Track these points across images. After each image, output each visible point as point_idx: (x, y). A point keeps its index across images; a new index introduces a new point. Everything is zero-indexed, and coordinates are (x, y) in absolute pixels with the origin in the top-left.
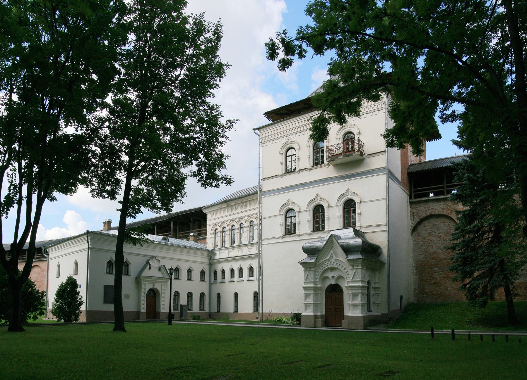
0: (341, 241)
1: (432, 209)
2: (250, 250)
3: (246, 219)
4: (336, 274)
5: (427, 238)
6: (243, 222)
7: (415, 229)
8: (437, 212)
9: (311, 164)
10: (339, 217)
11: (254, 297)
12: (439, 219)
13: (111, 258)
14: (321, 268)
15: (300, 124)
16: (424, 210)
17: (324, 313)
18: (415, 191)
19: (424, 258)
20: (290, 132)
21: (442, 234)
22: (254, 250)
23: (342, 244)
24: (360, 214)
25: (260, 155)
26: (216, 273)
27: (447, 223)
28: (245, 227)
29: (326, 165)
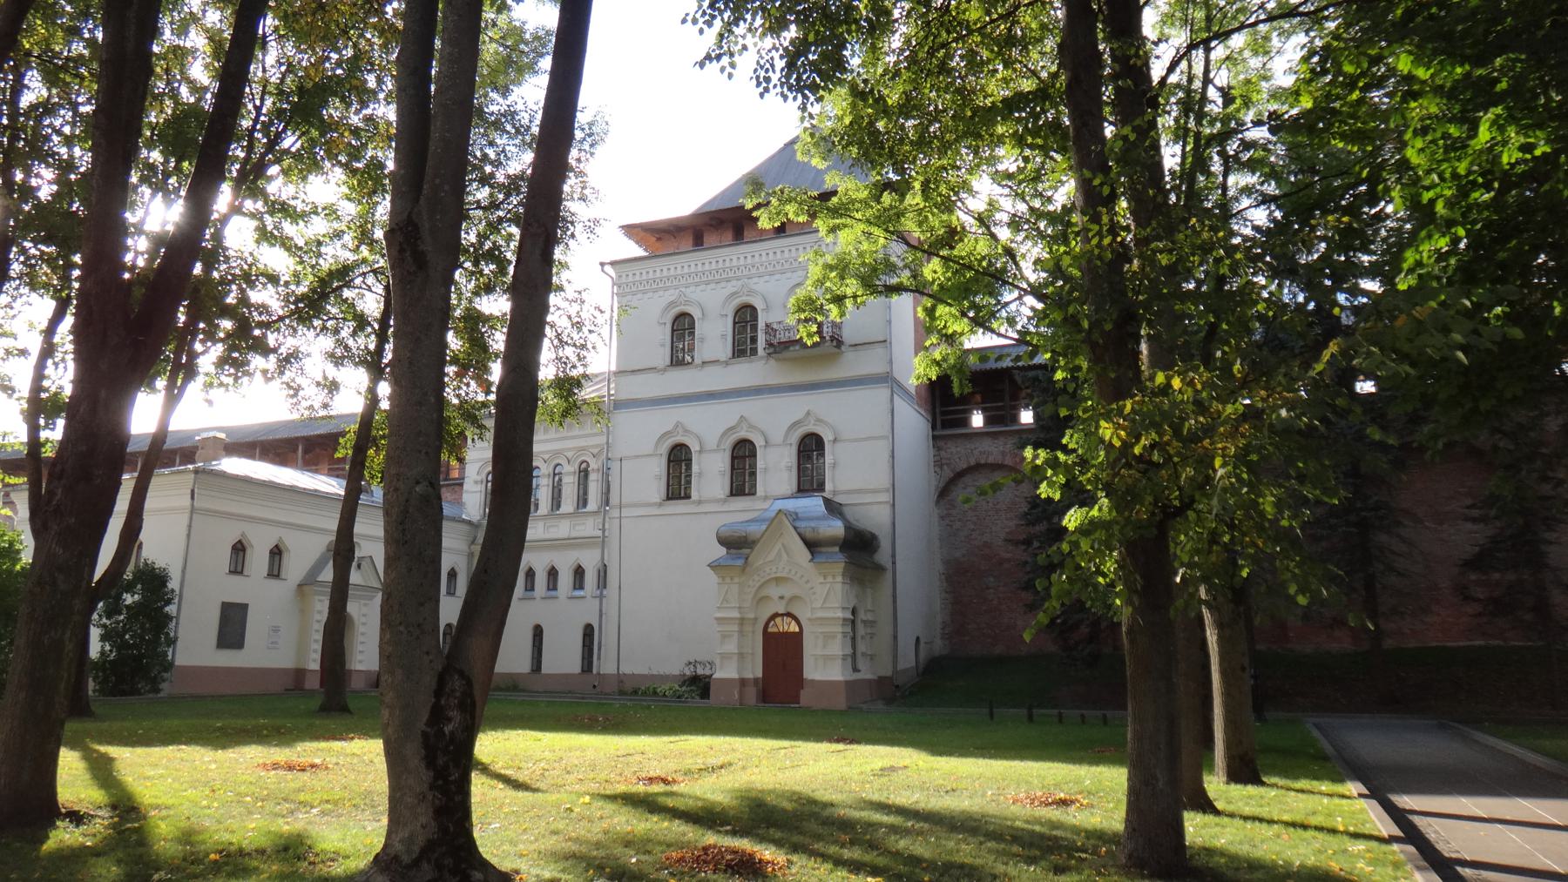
3: (570, 454)
4: (787, 591)
6: (563, 461)
7: (944, 493)
8: (991, 460)
9: (730, 354)
10: (789, 468)
11: (585, 635)
15: (707, 267)
17: (760, 675)
18: (943, 413)
22: (588, 528)
24: (834, 465)
28: (568, 474)
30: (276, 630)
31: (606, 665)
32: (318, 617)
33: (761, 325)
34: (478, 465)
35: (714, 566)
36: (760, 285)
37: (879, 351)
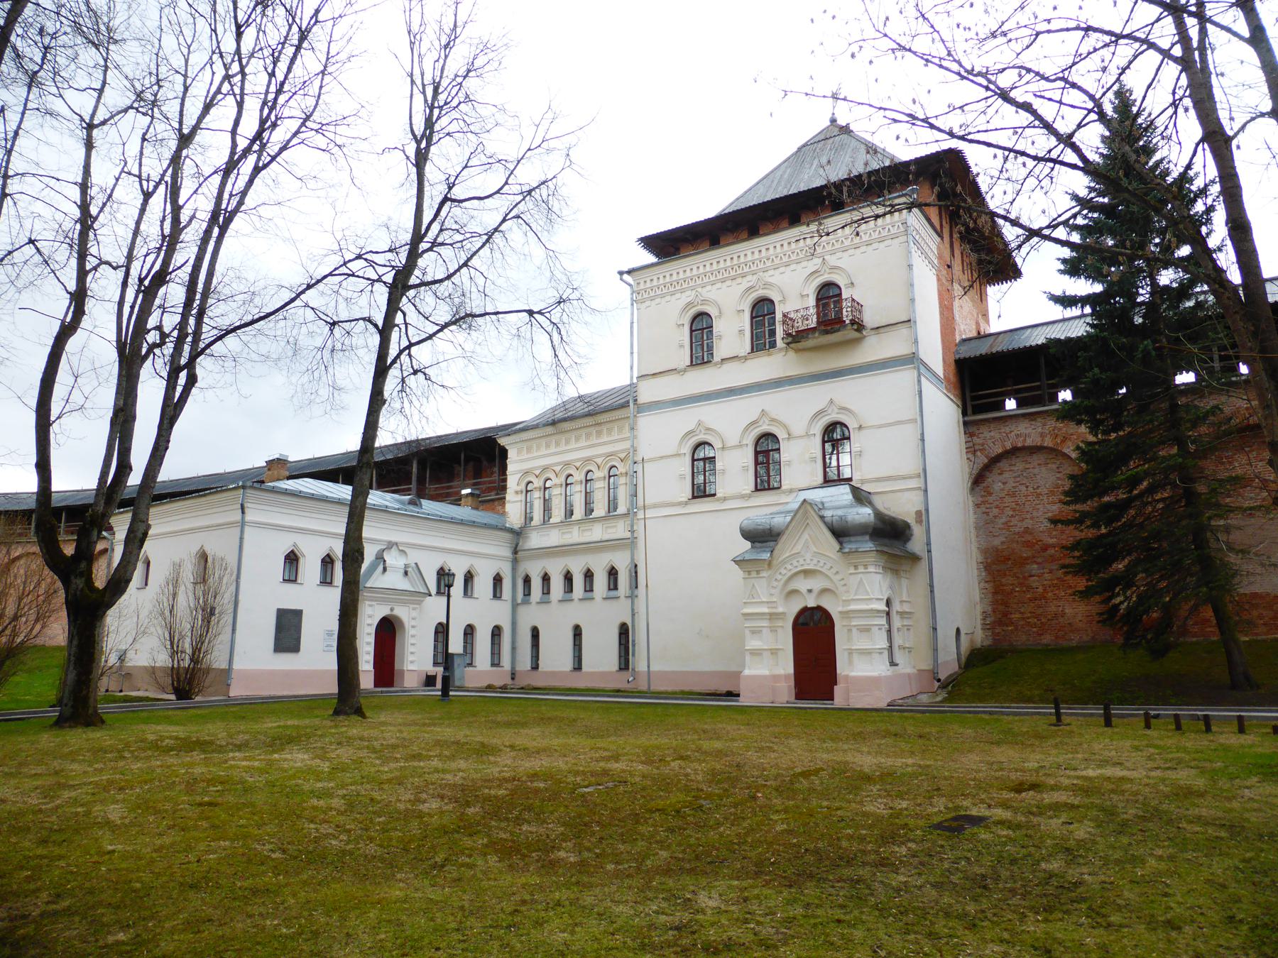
1: (1017, 436)
2: (610, 531)
4: (816, 584)
5: (1008, 499)
7: (978, 480)
8: (1029, 442)
9: (748, 349)
11: (620, 634)
12: (1035, 456)
13: (331, 549)
16: (995, 440)
18: (973, 399)
19: (1003, 543)
20: (699, 282)
21: (1041, 493)
22: (619, 530)
25: (632, 327)
26: (527, 580)
27: (1054, 466)
28: (599, 479)
29: (781, 349)
32: (369, 621)
33: (779, 316)
35: (739, 562)
36: (775, 277)
37: (904, 331)
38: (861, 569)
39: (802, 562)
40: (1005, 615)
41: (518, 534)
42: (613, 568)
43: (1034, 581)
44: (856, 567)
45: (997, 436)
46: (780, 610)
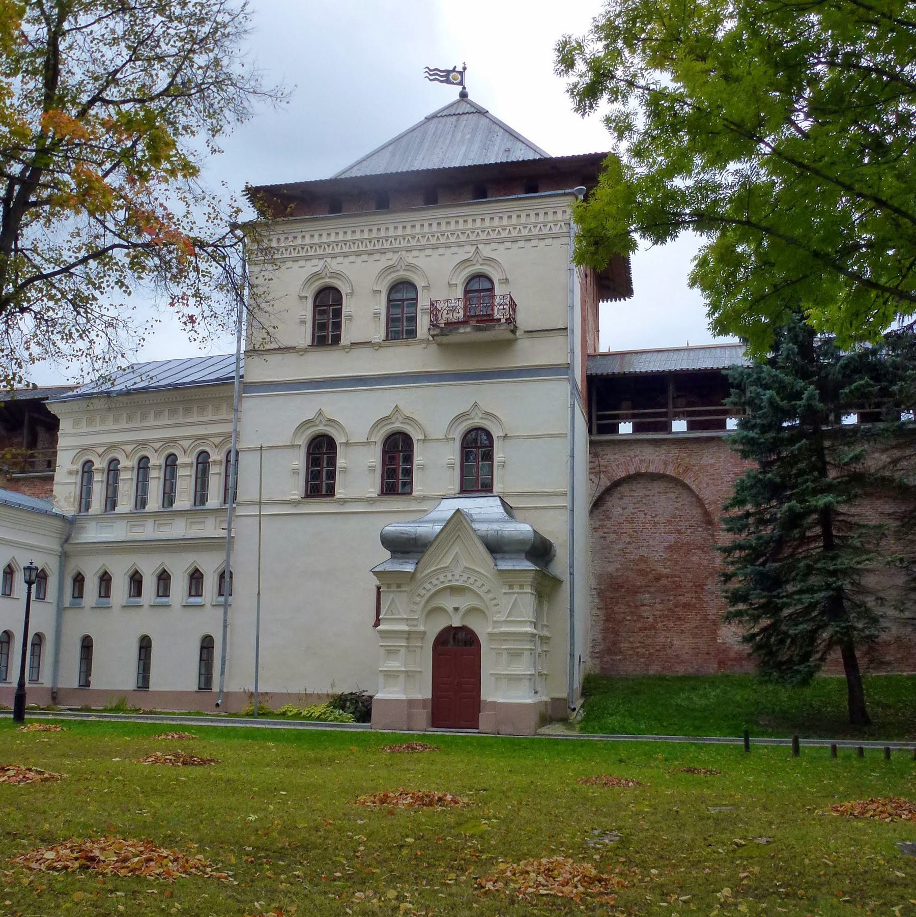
0: (482, 527)
7: (598, 504)
8: (652, 469)
12: (655, 484)
14: (428, 586)
18: (600, 418)
19: (617, 570)
22: (210, 529)
23: (484, 533)
26: (79, 580)
27: (673, 496)
30: (231, 595)
31: (235, 679)
34: (73, 453)
36: (499, 253)
37: (559, 339)
38: (516, 590)
39: (449, 577)
40: (614, 644)
41: (70, 524)
42: (106, 573)
43: (645, 611)
44: (511, 587)
45: (622, 459)
46: (422, 628)
